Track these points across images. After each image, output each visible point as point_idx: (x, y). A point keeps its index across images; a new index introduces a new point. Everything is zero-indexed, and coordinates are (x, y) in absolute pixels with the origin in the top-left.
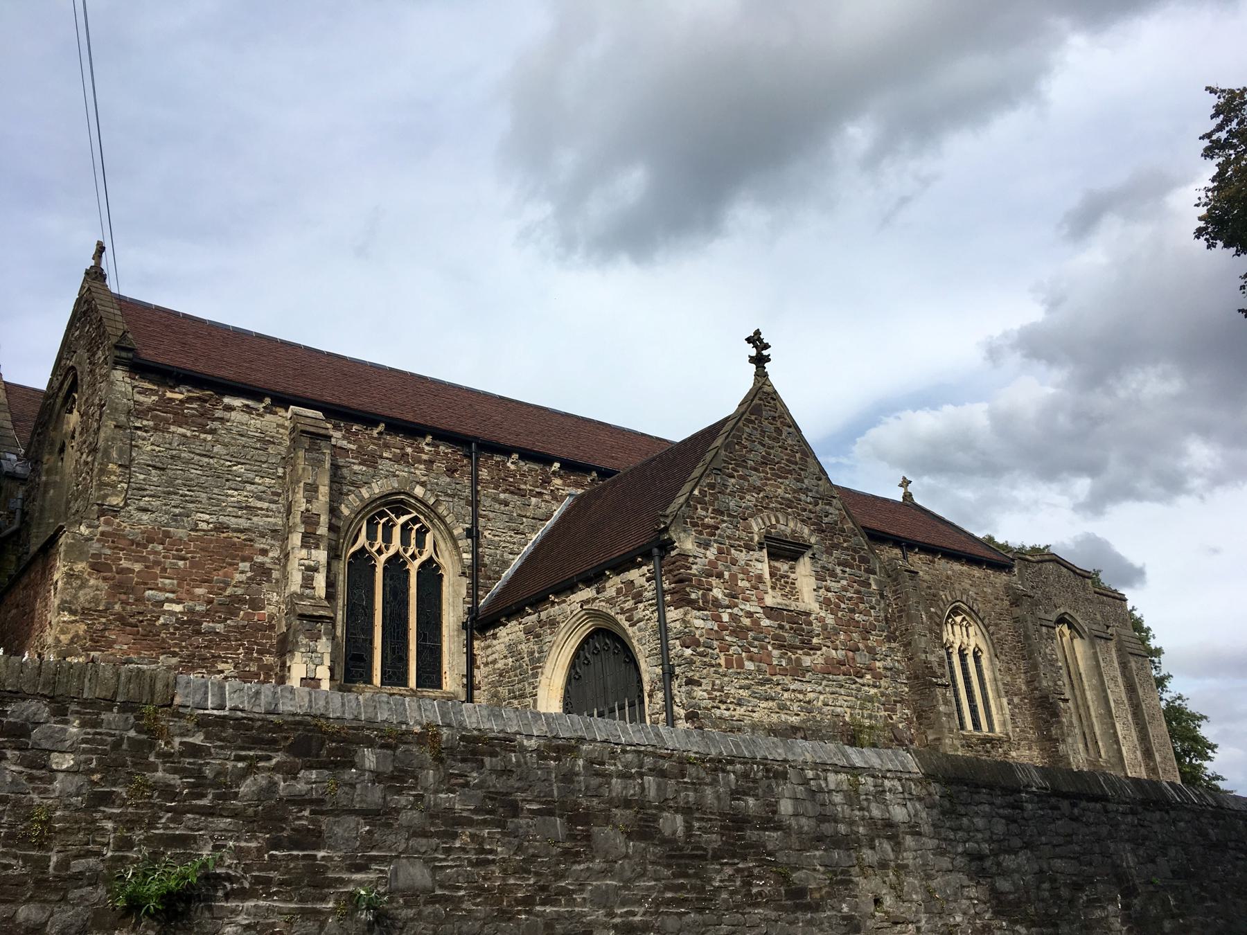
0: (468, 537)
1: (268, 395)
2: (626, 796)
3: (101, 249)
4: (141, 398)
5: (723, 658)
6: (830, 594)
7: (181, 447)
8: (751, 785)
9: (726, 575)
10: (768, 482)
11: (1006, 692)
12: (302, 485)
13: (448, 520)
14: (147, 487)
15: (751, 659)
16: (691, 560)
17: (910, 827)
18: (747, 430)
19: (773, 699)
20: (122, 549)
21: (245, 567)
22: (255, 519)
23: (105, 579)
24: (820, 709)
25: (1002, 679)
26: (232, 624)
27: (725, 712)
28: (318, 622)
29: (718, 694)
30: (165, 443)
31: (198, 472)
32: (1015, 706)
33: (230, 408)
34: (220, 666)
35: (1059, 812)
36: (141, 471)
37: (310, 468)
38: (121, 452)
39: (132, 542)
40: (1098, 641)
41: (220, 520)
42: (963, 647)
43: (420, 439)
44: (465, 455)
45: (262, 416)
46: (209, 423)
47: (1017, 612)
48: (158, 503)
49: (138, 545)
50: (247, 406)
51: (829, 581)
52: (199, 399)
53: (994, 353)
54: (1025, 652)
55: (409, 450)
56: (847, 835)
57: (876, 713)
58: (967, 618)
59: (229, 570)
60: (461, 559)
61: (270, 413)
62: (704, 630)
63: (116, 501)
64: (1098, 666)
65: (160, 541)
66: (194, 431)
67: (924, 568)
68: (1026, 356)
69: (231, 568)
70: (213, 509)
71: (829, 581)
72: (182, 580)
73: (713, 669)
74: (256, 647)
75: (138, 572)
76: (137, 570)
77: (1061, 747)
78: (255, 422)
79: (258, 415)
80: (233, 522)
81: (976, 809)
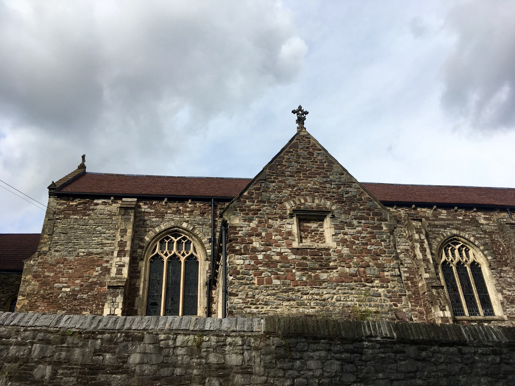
0: (210, 242)
1: (112, 196)
2: (18, 356)
3: (83, 157)
4: (60, 207)
5: (256, 279)
6: (346, 237)
7: (74, 223)
8: (113, 346)
9: (264, 234)
10: (301, 181)
12: (119, 230)
13: (200, 236)
14: (59, 241)
15: (278, 278)
16: (238, 229)
17: (242, 369)
18: (286, 157)
19: (294, 300)
20: (46, 268)
21: (98, 269)
22: (105, 248)
23: (38, 281)
24: (333, 305)
26: (91, 294)
27: (255, 309)
28: (117, 289)
29: (250, 300)
30: (68, 223)
31: (81, 232)
33: (97, 204)
34: (84, 313)
35: (403, 355)
36: (56, 236)
37: (124, 222)
38: (50, 229)
39: (51, 264)
41: (89, 251)
43: (186, 202)
45: (111, 205)
46: (87, 212)
48: (63, 247)
49: (53, 265)
50: (104, 202)
51: (346, 229)
52: (83, 203)
55: (181, 208)
56: (181, 376)
59: (91, 271)
60: (206, 253)
61: (114, 203)
62: (243, 266)
63: (45, 249)
65: (62, 263)
66: (80, 216)
69: (92, 270)
70: (86, 246)
71: (346, 229)
72: (70, 278)
73: (247, 286)
74: (101, 303)
75: (52, 277)
76: (51, 276)
78: (108, 208)
79: (109, 205)
80: (94, 251)
81: (312, 354)
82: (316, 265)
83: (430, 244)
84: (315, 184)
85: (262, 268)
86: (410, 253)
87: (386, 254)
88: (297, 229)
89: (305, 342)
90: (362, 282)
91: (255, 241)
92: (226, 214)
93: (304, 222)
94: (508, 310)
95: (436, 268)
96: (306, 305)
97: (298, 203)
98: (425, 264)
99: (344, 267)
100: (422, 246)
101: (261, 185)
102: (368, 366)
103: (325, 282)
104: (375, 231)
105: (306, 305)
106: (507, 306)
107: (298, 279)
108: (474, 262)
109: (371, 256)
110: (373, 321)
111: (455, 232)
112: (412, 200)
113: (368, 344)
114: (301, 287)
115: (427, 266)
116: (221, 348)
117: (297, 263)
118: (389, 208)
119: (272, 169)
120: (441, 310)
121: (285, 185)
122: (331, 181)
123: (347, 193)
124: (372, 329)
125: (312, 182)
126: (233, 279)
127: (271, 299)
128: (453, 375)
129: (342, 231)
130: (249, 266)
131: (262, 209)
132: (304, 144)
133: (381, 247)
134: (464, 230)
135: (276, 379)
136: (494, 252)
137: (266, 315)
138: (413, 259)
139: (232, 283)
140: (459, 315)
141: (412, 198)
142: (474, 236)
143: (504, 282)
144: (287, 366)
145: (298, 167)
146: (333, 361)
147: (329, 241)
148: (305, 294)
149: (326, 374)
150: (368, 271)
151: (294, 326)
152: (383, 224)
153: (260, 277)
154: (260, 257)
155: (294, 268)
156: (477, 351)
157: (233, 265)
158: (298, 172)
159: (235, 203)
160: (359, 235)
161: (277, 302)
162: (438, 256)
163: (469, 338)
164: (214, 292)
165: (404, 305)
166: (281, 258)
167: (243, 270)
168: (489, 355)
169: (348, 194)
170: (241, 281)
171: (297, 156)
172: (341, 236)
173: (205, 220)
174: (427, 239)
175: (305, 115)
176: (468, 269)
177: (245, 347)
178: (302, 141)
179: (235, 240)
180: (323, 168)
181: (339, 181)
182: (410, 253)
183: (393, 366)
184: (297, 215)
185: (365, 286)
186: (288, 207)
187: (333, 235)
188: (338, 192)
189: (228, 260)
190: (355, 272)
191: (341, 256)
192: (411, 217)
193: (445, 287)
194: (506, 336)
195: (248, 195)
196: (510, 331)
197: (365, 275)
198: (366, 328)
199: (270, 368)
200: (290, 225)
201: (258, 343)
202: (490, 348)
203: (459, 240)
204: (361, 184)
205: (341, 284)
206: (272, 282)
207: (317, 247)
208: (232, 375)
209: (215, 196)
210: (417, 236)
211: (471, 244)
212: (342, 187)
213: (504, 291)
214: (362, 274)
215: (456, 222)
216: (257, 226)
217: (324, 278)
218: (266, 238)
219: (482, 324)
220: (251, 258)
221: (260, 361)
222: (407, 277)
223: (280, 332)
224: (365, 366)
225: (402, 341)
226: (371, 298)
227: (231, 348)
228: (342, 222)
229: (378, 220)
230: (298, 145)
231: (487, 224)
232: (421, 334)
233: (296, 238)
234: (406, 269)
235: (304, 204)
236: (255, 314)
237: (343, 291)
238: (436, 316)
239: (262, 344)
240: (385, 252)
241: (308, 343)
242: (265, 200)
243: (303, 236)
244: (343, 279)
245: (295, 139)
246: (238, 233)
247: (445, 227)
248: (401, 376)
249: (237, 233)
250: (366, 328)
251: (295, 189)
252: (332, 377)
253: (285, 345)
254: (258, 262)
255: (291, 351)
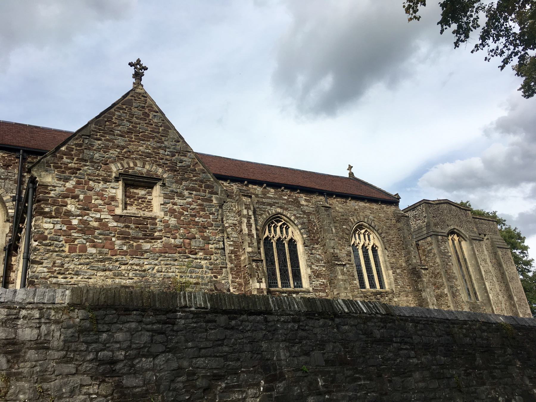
0: (13, 201)
5: (67, 246)
6: (175, 207)
9: (81, 197)
10: (132, 143)
11: (392, 267)
15: (94, 246)
16: (49, 188)
18: (117, 113)
24: (154, 276)
25: (389, 261)
27: (62, 280)
29: (57, 269)
32: (398, 275)
40: (474, 241)
42: (366, 245)
44: (16, 157)
47: (399, 225)
51: (176, 199)
53: (487, 132)
54: (404, 246)
57: (204, 275)
58: (368, 230)
60: (7, 213)
62: (53, 230)
64: (475, 254)
67: (339, 206)
68: (502, 133)
73: (55, 254)
77: (423, 294)
82: (140, 234)
83: (256, 221)
84: (147, 148)
85: (76, 235)
86: (237, 228)
87: (213, 227)
88: (123, 195)
89: (115, 314)
90: (186, 253)
91: (71, 204)
92: (36, 169)
93: (131, 188)
94: (313, 283)
95: (259, 243)
96: (124, 276)
97: (126, 166)
98: (249, 239)
99: (169, 237)
100: (248, 221)
101: (83, 141)
102: (178, 336)
103: (148, 252)
104: (205, 203)
105: (124, 276)
106: (314, 280)
107: (118, 248)
108: (292, 239)
109: (198, 228)
110: (191, 293)
111: (279, 210)
112: (246, 176)
113: (182, 314)
114: (120, 256)
115: (251, 241)
116: (13, 321)
117: (118, 230)
118: (223, 182)
119: (99, 125)
120: (258, 282)
121: (113, 144)
122: (165, 147)
123: (181, 162)
124: (187, 300)
125: (144, 146)
126: (37, 245)
127: (83, 268)
128: (257, 342)
129: (172, 200)
130: (60, 231)
131: (82, 169)
132: (139, 102)
133: (209, 220)
134: (286, 209)
135: (77, 353)
136: (309, 232)
137: (75, 286)
138: (239, 233)
139: (35, 249)
140: (273, 287)
141: (245, 174)
142: (294, 215)
143: (314, 258)
144: (91, 339)
145: (130, 127)
146: (143, 332)
147: (157, 211)
148: (124, 264)
149: (134, 346)
150: (193, 243)
151: (105, 298)
152: (213, 197)
153: (72, 245)
154: (75, 222)
155: (114, 236)
156: (280, 320)
157: (39, 229)
158: (130, 132)
159: (48, 158)
160: (189, 206)
161: (90, 272)
162: (262, 232)
163: (275, 307)
164: (13, 259)
165: (224, 277)
166: (100, 224)
167: (52, 235)
168: (290, 322)
169: (182, 162)
170: (49, 248)
171: (129, 114)
172: (170, 206)
173: (9, 174)
174: (254, 215)
175: (143, 70)
176: (286, 245)
177: (43, 320)
178: (137, 99)
179: (45, 201)
180: (158, 133)
181: (174, 149)
182: (237, 228)
183: (203, 334)
184: (124, 180)
185: (189, 257)
186: (114, 169)
187: (161, 204)
188: (171, 160)
189: (33, 223)
190: (180, 244)
191: (167, 226)
192: (243, 192)
193: (264, 261)
194: (306, 306)
195: (66, 150)
196: (309, 302)
197: (190, 246)
198: (182, 299)
199: (71, 342)
200: (115, 190)
201: (60, 315)
202: (291, 317)
203: (281, 218)
204: (196, 154)
205: (164, 254)
206: (86, 250)
207: (142, 215)
208: (24, 350)
209: (24, 147)
210: (245, 212)
211: (291, 223)
212: (177, 155)
213: (313, 266)
214: (187, 245)
215: (281, 201)
216: (75, 187)
217: (147, 248)
218: (84, 202)
219: (291, 295)
220: (63, 223)
221: (60, 335)
222: (232, 251)
223: (87, 304)
224: (176, 336)
225: (215, 311)
226: (193, 270)
227: (26, 322)
228: (172, 191)
229: (209, 193)
230: (132, 102)
231: (307, 206)
232: (233, 304)
233: (120, 204)
234: (232, 243)
235: (133, 168)
236: (62, 284)
237: (166, 262)
238: (253, 288)
239: (65, 317)
240: (212, 224)
241: (118, 315)
242: (87, 158)
243: (128, 202)
244: (167, 249)
245: (130, 95)
246: (49, 193)
247: (271, 205)
248: (209, 344)
249: (47, 192)
250: (182, 299)
251: (125, 150)
252: (140, 348)
253: (91, 317)
254: (71, 227)
255: (97, 323)
